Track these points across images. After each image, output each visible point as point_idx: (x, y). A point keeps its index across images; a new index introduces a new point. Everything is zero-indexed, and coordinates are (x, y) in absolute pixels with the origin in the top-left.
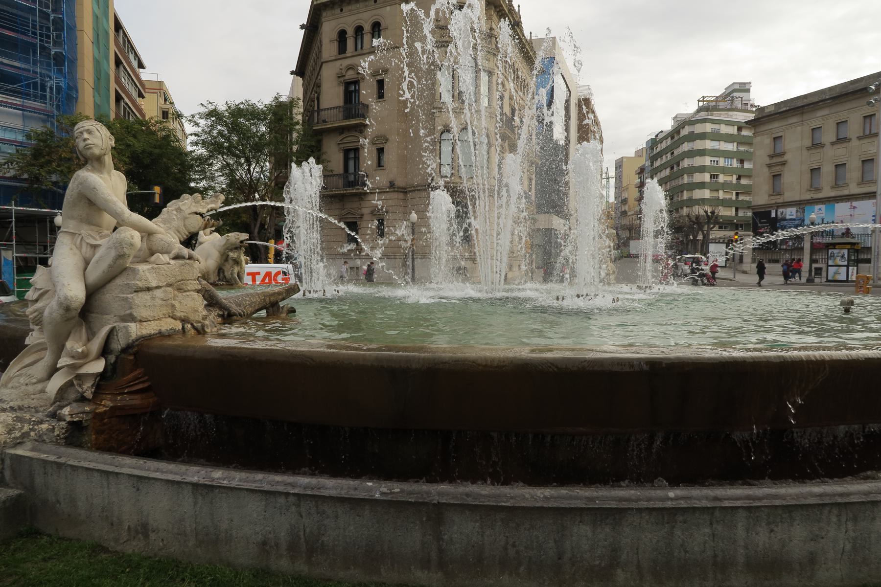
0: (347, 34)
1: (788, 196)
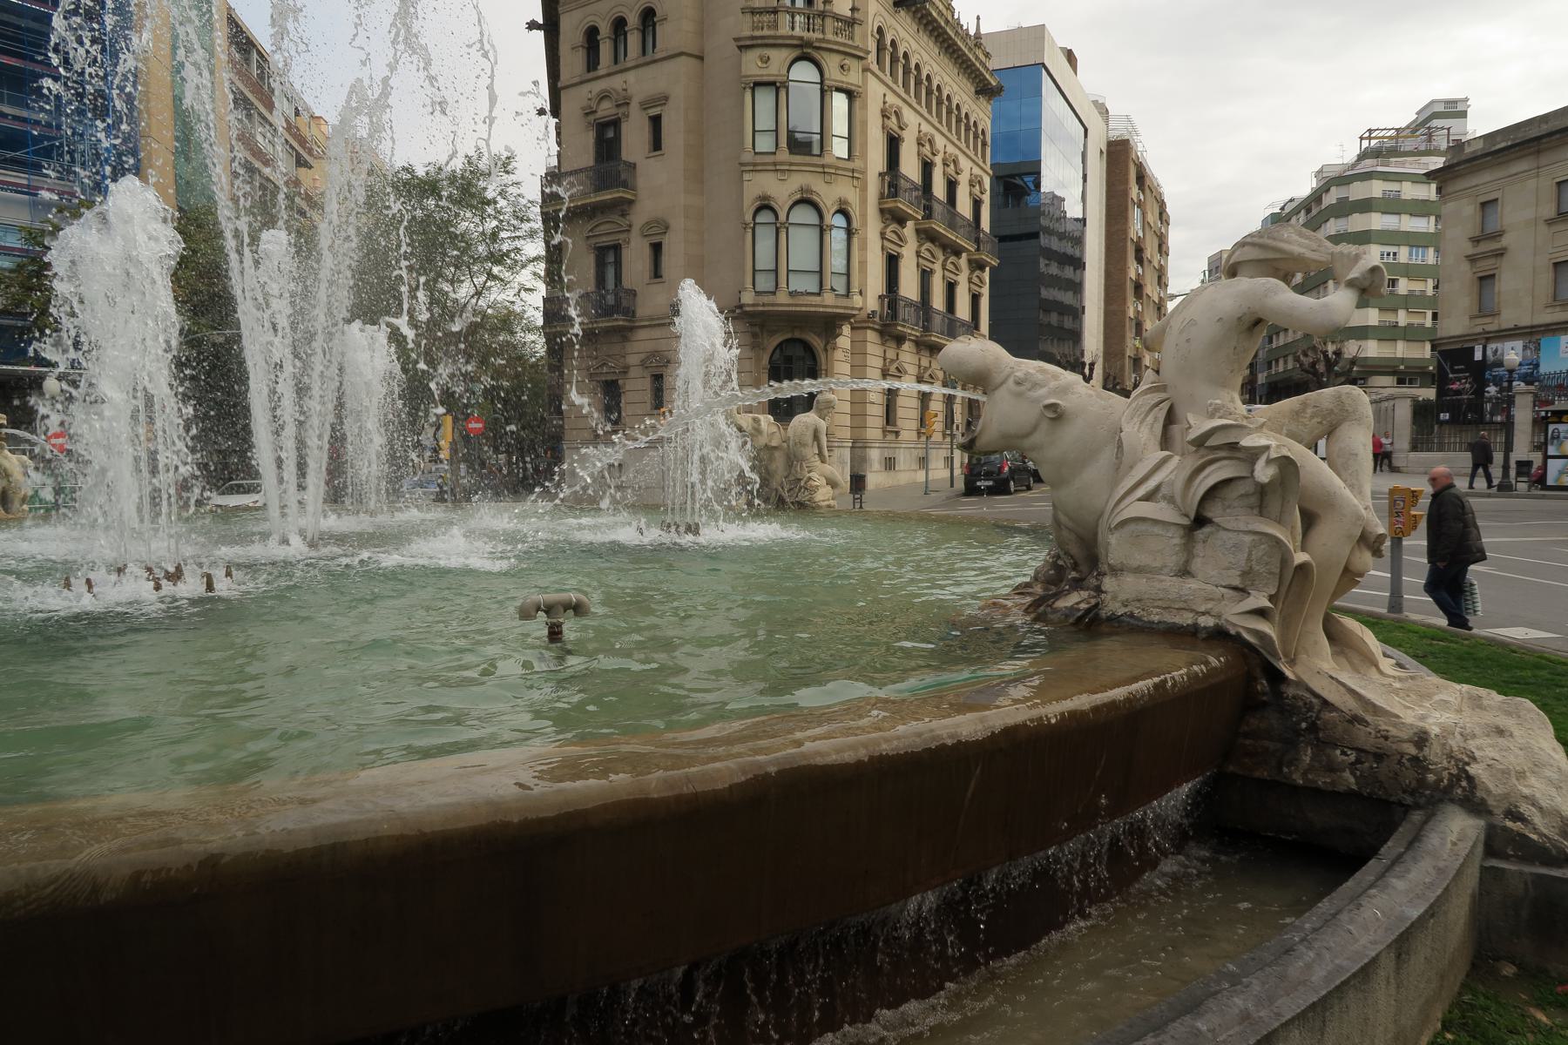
0: (626, 24)
1: (1510, 317)
